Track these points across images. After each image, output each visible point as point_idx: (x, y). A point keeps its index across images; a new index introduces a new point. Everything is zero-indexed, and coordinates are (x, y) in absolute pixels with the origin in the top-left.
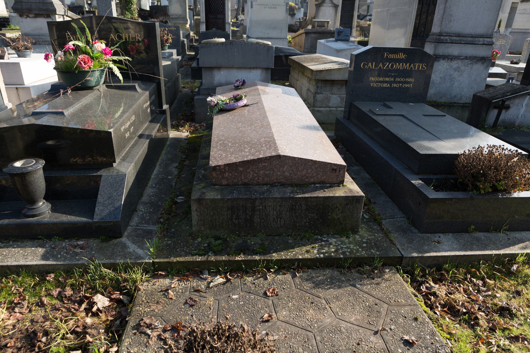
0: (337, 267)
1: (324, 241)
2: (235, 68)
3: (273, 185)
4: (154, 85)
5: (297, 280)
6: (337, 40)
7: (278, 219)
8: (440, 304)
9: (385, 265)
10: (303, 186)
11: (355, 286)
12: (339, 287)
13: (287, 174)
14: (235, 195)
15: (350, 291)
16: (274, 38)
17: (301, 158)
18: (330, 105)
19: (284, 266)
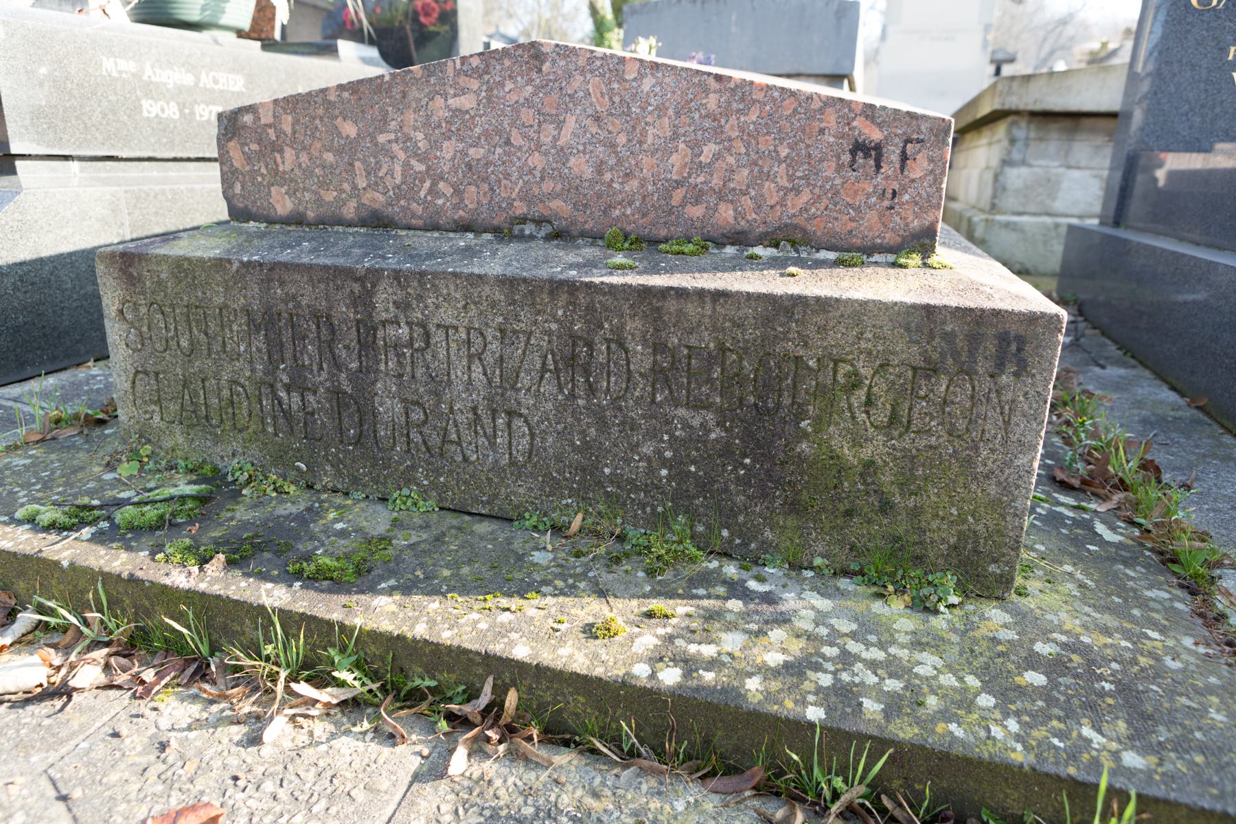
7: (494, 414)
13: (581, 166)
19: (413, 688)
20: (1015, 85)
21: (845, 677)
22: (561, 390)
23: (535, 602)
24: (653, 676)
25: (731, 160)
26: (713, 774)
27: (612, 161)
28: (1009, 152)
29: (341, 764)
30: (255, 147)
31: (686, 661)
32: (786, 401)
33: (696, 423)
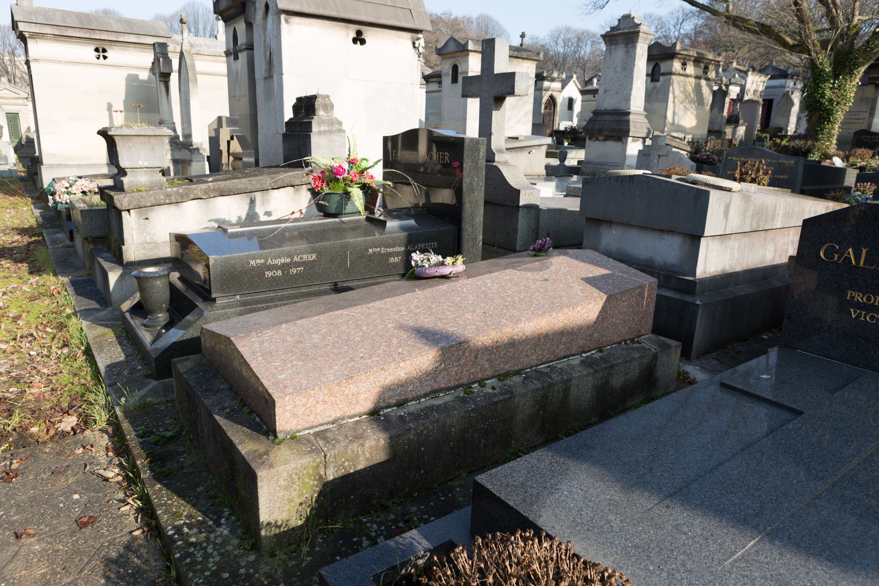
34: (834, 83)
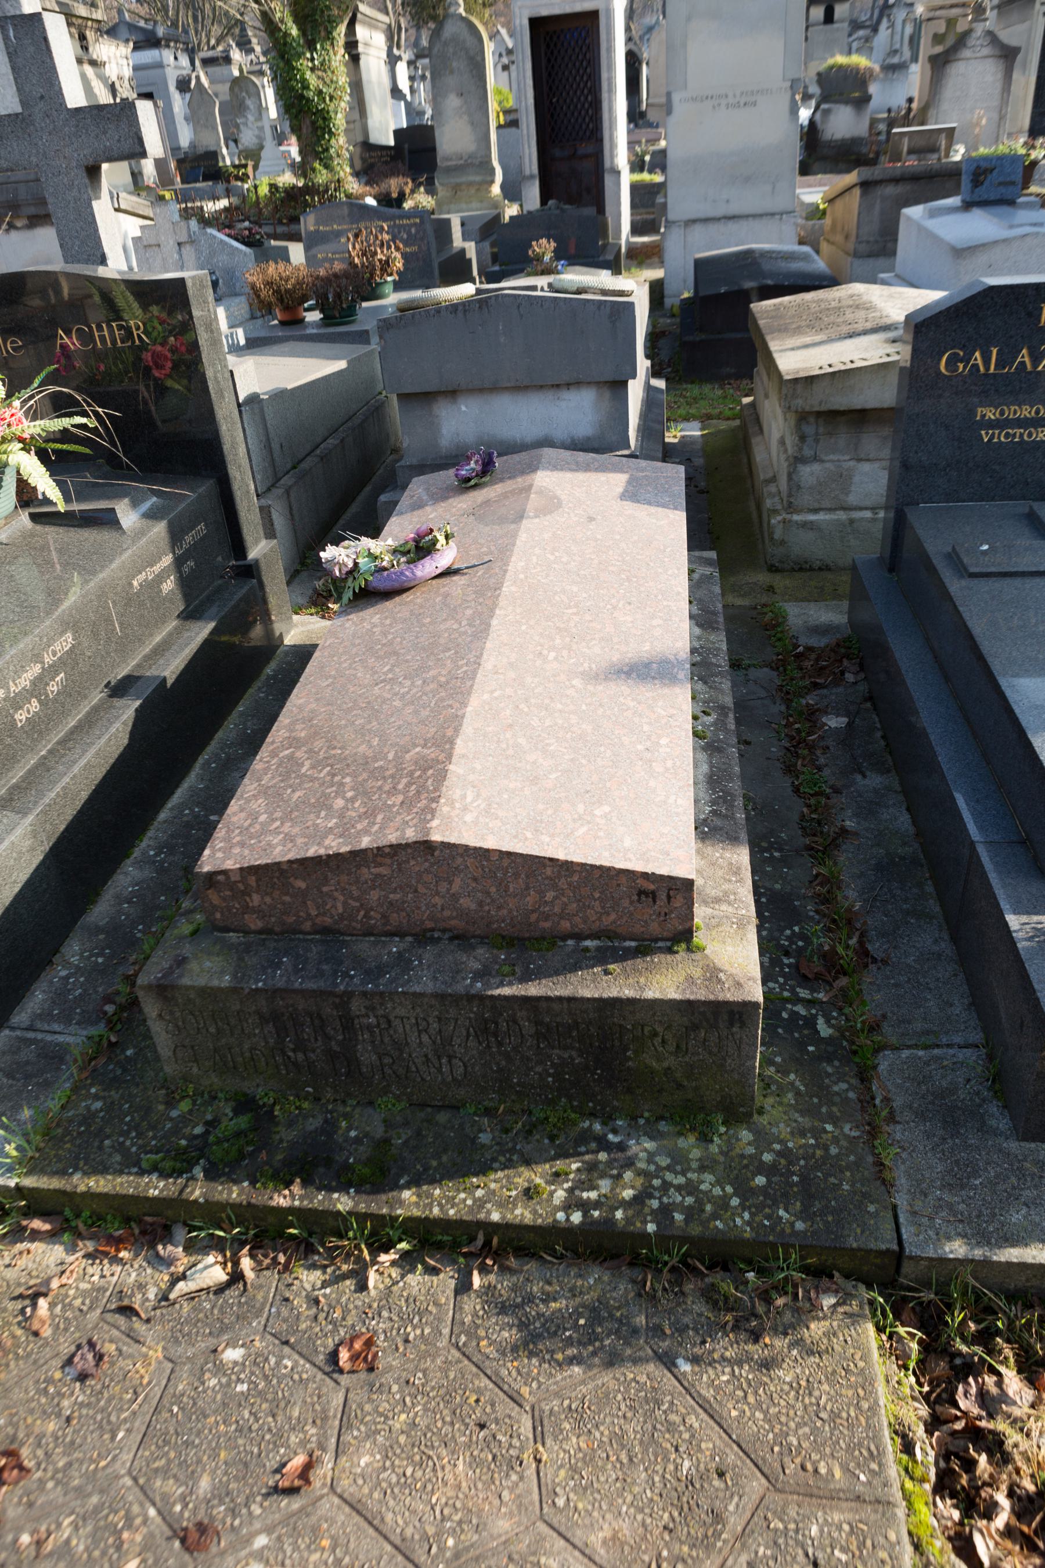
0: (631, 1264)
1: (607, 1147)
2: (507, 388)
3: (423, 938)
4: (189, 495)
5: (471, 1304)
6: (968, 206)
7: (439, 1058)
8: (1011, 1494)
9: (820, 1274)
10: (532, 945)
11: (668, 1361)
12: (612, 1360)
13: (466, 903)
14: (279, 978)
15: (641, 1387)
16: (747, 217)
17: (509, 854)
18: (852, 499)
19: (435, 1242)
20: (799, 387)
21: (665, 1200)
22: (480, 1043)
23: (492, 1177)
24: (568, 1219)
25: (565, 900)
26: (605, 1260)
27: (488, 900)
28: (801, 449)
29: (415, 1291)
30: (228, 893)
31: (583, 1205)
32: (617, 1043)
33: (566, 1055)
34: (312, 59)
